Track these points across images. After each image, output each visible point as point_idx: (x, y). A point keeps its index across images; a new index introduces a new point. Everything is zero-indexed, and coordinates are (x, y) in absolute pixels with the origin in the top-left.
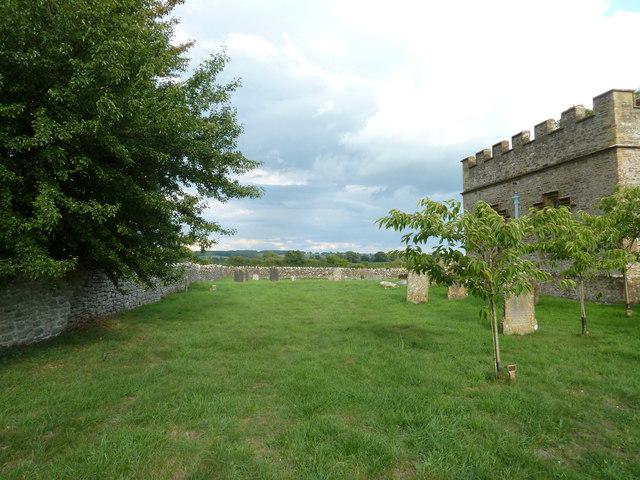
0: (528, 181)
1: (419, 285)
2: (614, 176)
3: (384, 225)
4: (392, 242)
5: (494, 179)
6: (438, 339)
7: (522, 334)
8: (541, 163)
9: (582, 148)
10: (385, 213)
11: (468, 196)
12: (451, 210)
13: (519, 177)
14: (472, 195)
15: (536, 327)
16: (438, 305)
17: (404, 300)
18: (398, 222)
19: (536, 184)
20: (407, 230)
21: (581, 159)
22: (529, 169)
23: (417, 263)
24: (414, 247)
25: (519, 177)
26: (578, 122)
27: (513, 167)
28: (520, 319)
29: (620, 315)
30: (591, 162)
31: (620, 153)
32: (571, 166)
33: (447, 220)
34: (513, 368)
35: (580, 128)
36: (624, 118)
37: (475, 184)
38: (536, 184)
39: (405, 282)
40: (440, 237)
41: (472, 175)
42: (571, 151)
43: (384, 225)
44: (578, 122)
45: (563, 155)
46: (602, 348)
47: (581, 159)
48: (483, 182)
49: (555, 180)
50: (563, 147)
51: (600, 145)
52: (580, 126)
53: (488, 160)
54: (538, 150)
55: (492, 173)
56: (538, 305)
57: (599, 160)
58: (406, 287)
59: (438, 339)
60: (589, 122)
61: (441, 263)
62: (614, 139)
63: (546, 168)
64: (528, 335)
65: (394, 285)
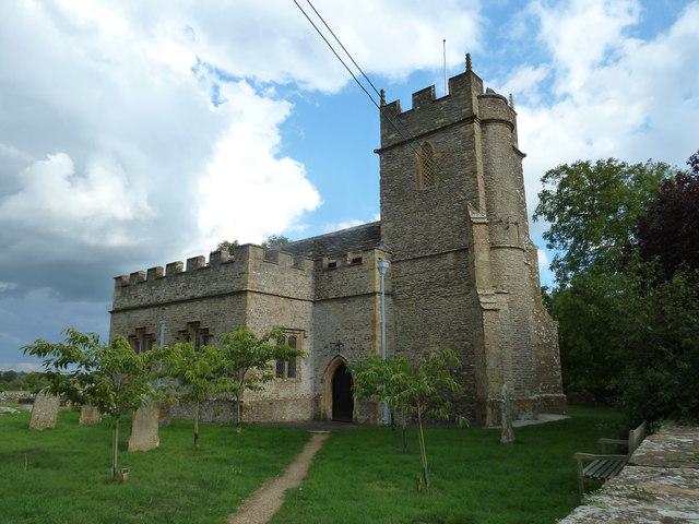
0: (175, 309)
1: (47, 408)
2: (243, 316)
3: (28, 352)
4: (34, 366)
5: (145, 302)
6: (63, 459)
7: (145, 450)
8: (190, 293)
9: (223, 286)
10: (31, 342)
11: (116, 316)
12: (91, 341)
13: (169, 304)
14: (122, 315)
15: (158, 444)
16: (67, 431)
17: (26, 427)
18: (41, 351)
19: (183, 313)
20: (49, 356)
21: (221, 296)
22: (178, 298)
23: (57, 385)
24: (54, 370)
25: (169, 304)
26: (223, 264)
27: (164, 293)
28: (145, 437)
29: (230, 433)
30: (228, 300)
31: (249, 295)
32: (212, 301)
33: (87, 349)
34: (127, 471)
35: (223, 269)
36: (255, 268)
37: (126, 304)
38: (183, 313)
39: (29, 407)
40: (79, 363)
41: (124, 294)
42: (214, 287)
43: (28, 352)
44: (223, 264)
45: (207, 289)
46: (205, 457)
47: (221, 296)
48: (134, 303)
49: (199, 311)
50: (208, 283)
51: (236, 286)
52: (223, 267)
53: (141, 282)
54: (188, 282)
55: (143, 295)
56: (162, 427)
57: (234, 299)
58: (30, 415)
59: (63, 459)
60: (230, 265)
61: (77, 385)
62: (245, 284)
63: (192, 299)
64: (153, 451)
65: (13, 411)
